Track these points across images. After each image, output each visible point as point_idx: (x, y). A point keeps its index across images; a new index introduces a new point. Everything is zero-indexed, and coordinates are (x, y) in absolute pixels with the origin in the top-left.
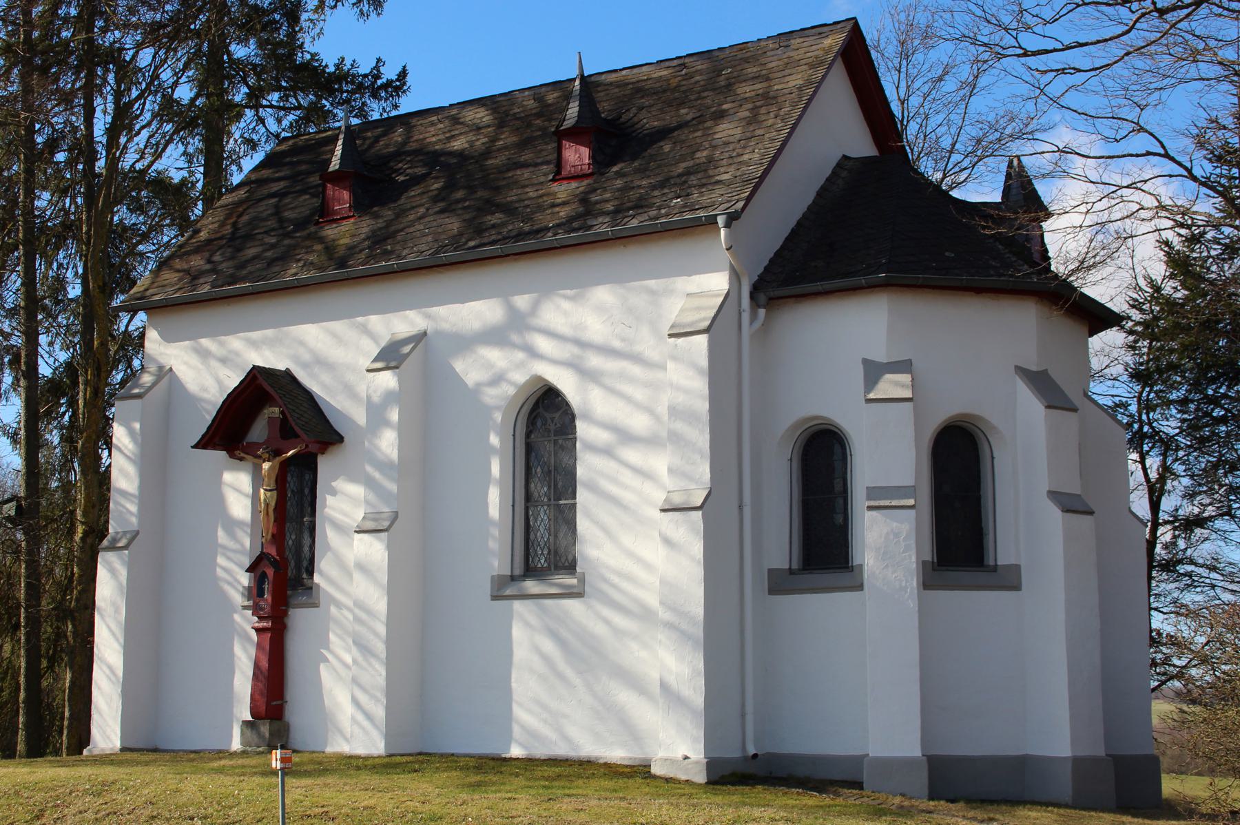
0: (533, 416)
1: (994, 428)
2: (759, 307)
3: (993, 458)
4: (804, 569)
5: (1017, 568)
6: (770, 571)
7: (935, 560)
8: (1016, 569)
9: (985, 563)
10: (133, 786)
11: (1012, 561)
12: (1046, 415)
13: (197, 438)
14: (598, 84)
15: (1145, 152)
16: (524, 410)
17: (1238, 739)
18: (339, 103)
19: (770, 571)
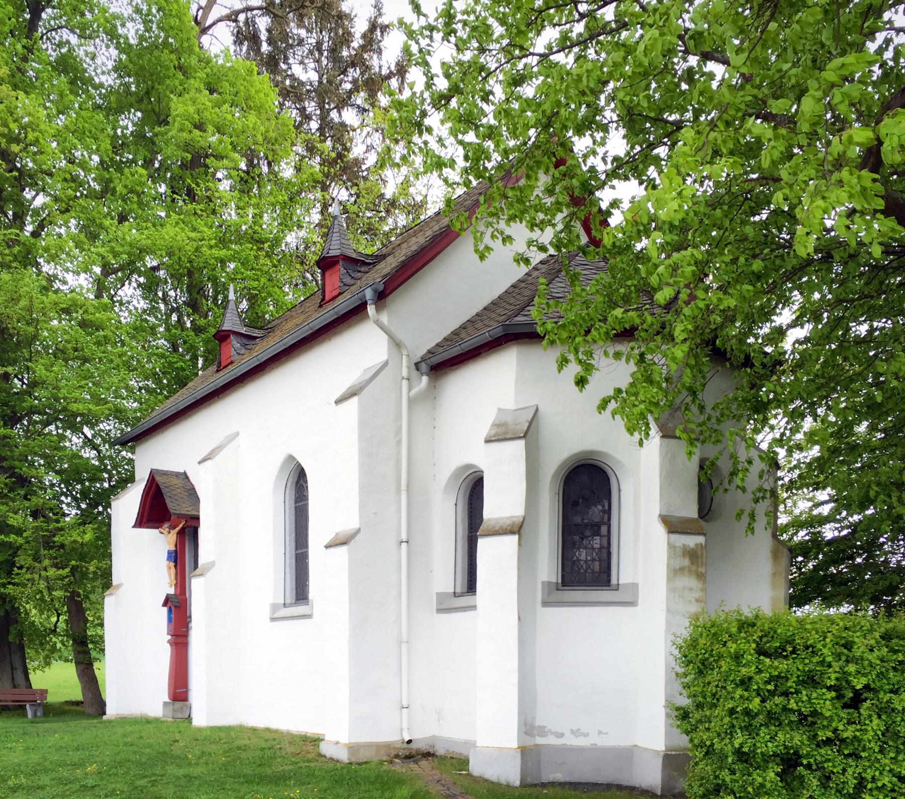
0: (67, 708)
1: (620, 462)
2: (422, 374)
3: (620, 490)
4: (468, 592)
5: (634, 587)
6: (437, 594)
7: (560, 581)
8: (634, 587)
9: (614, 581)
10: (243, 274)
11: (630, 581)
12: (661, 445)
13: (133, 523)
14: (175, 692)
15: (499, 332)
16: (289, 486)
17: (889, 733)
18: (235, 761)
19: (437, 594)
